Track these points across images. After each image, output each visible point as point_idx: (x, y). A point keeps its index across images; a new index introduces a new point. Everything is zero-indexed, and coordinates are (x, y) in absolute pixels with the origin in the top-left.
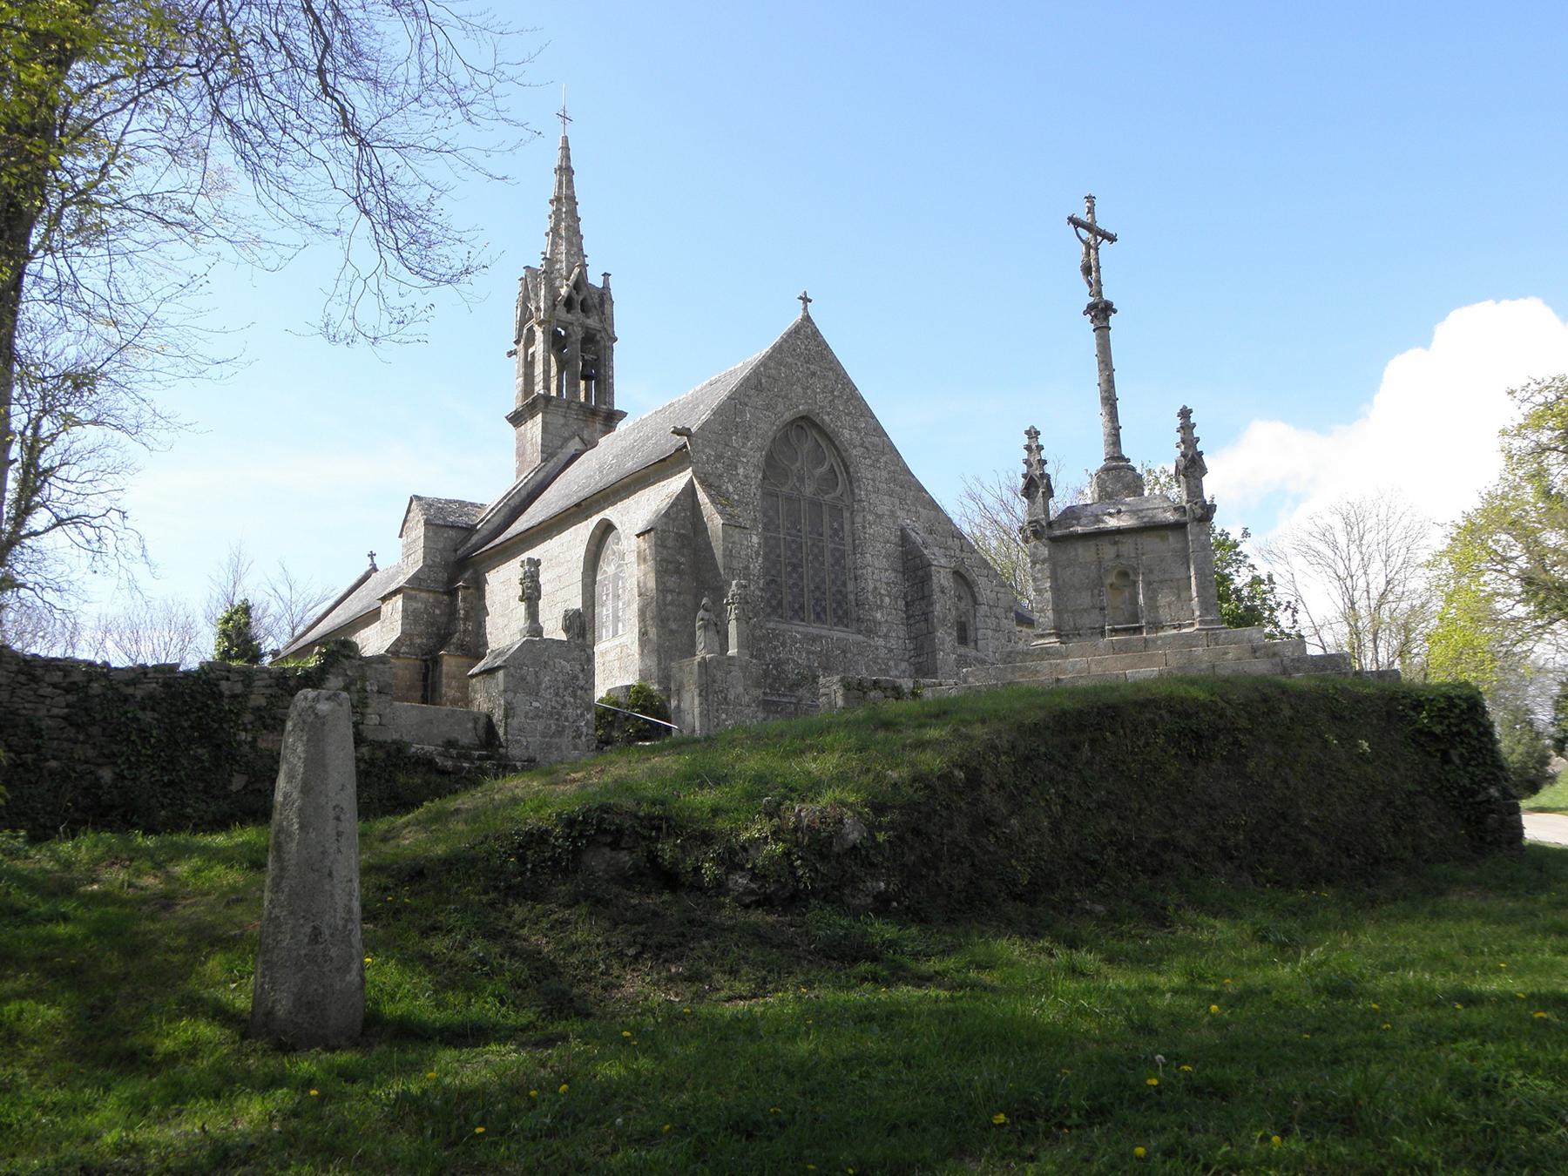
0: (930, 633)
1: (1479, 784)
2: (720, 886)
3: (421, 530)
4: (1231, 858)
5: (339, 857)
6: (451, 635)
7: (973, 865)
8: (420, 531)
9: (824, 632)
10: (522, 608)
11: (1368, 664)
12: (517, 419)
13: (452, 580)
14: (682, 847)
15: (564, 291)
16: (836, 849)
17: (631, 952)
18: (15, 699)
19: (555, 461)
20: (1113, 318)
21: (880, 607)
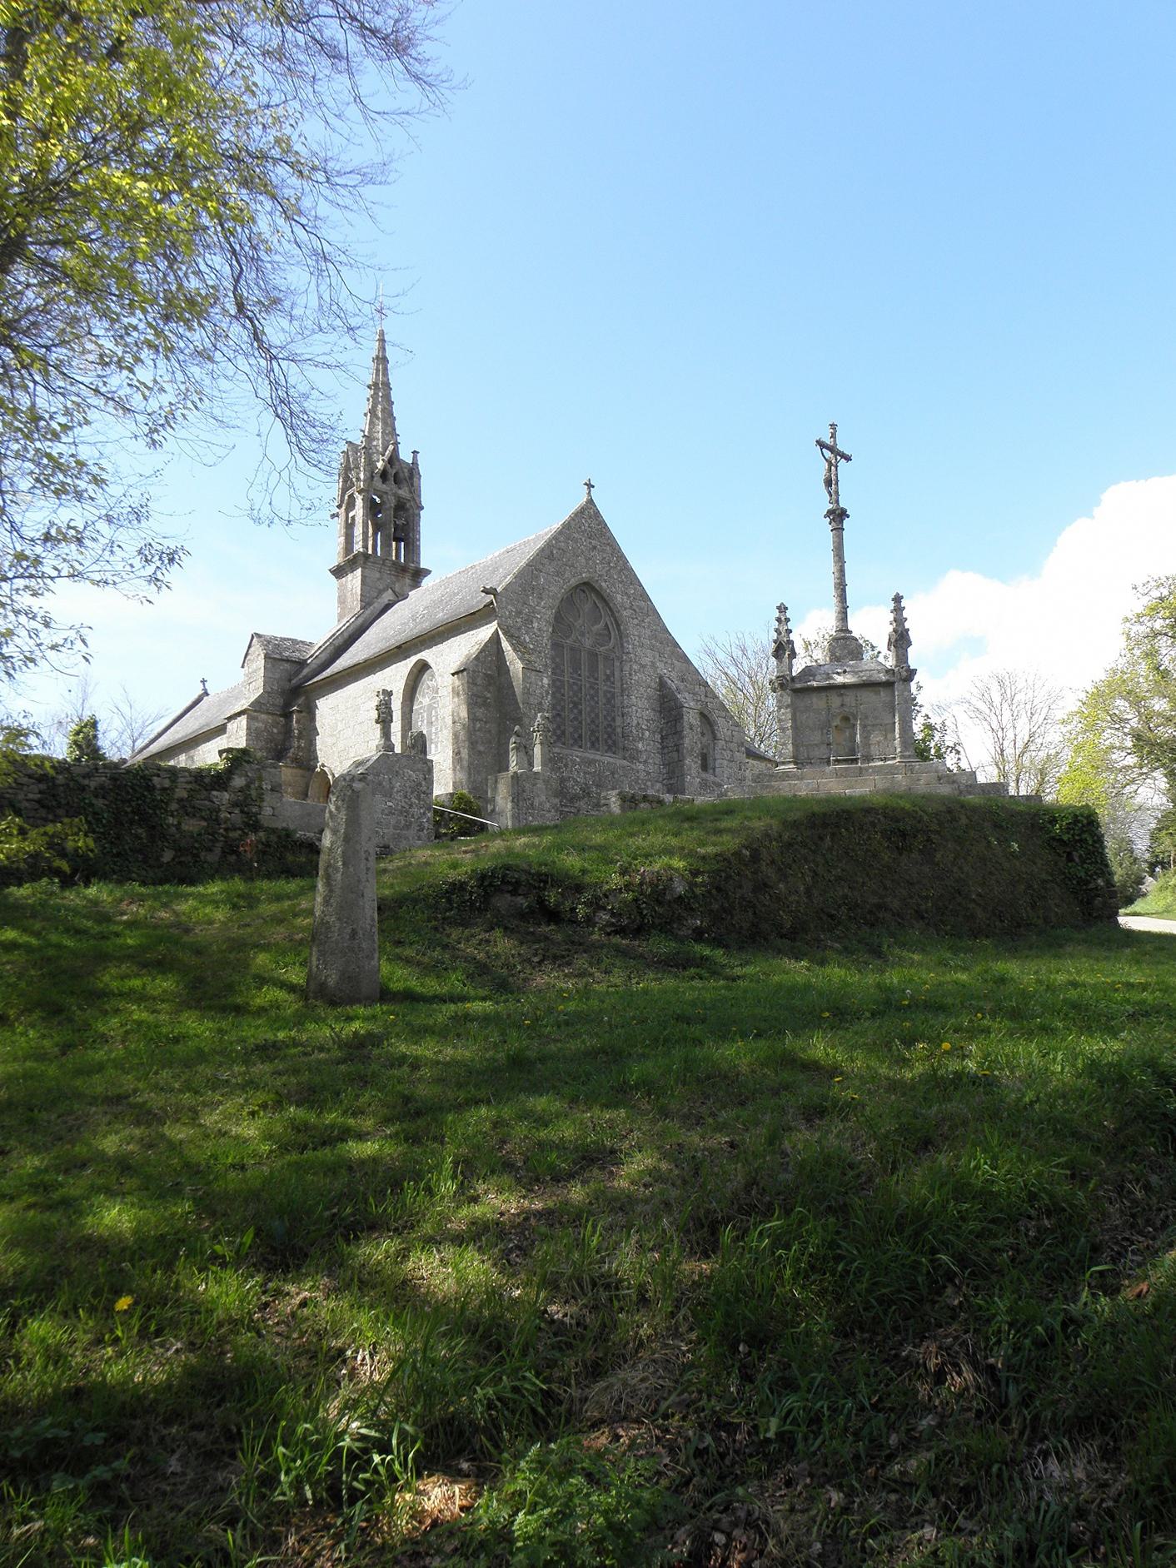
0: (681, 760)
1: (1091, 876)
2: (589, 921)
3: (261, 662)
4: (923, 918)
6: (287, 750)
7: (755, 913)
8: (260, 663)
9: (598, 757)
10: (377, 730)
12: (339, 572)
13: (288, 704)
14: (562, 894)
15: (380, 465)
16: (668, 897)
17: (536, 959)
19: (373, 609)
20: (846, 522)
21: (641, 739)
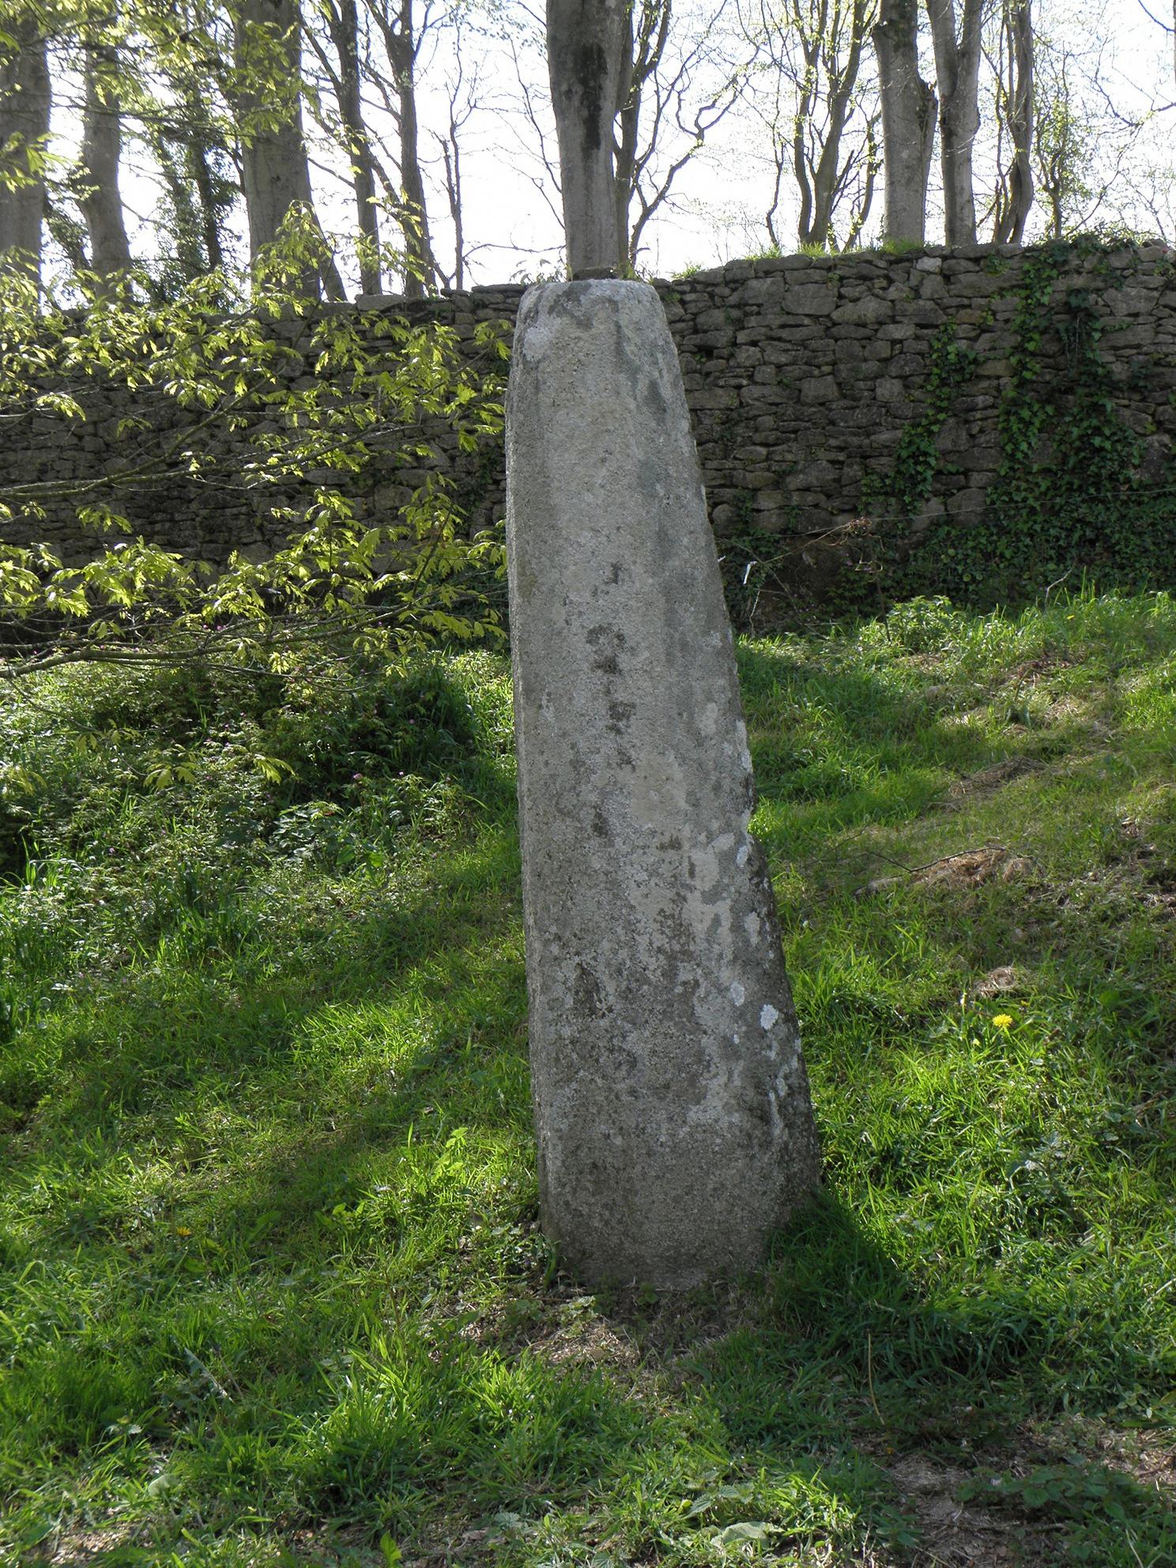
5: (625, 775)
11: (786, 253)
18: (1161, 338)
